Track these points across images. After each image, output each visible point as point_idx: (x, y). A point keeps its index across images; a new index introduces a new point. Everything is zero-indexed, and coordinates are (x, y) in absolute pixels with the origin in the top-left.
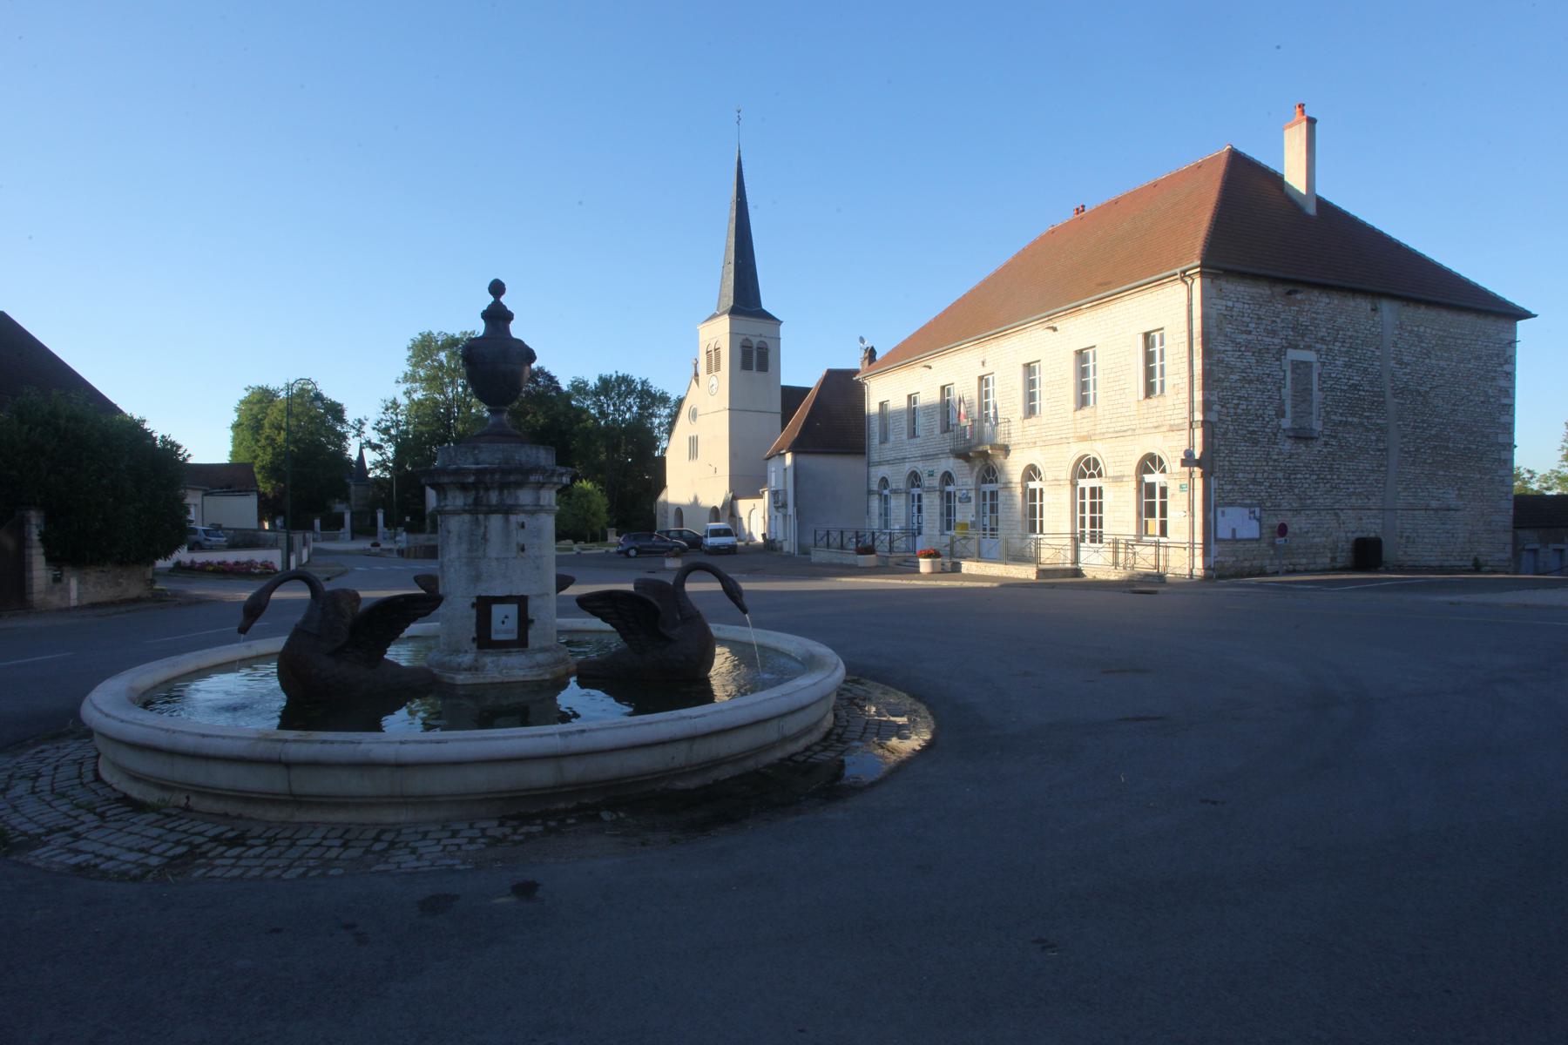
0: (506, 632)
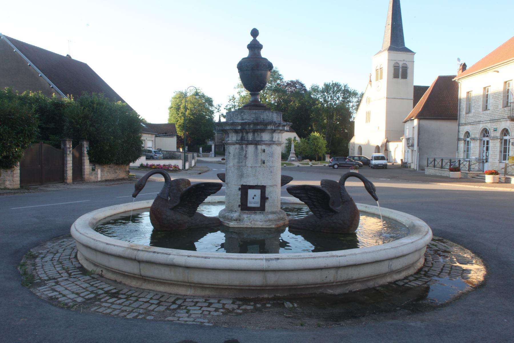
0: (255, 203)
